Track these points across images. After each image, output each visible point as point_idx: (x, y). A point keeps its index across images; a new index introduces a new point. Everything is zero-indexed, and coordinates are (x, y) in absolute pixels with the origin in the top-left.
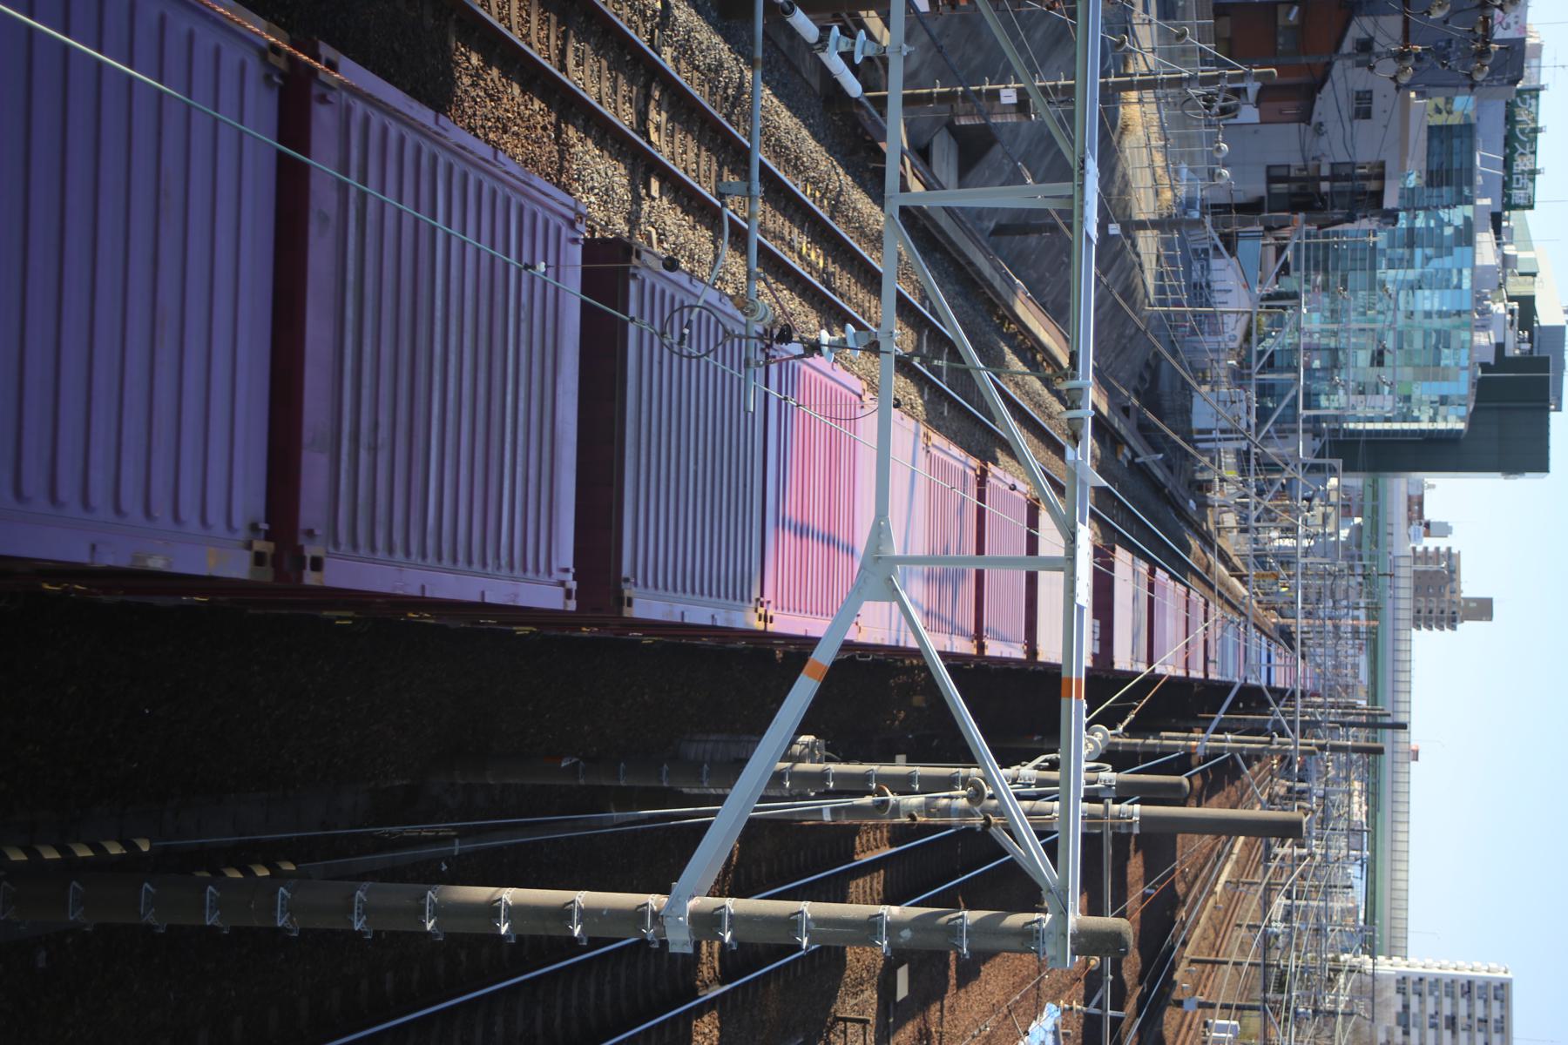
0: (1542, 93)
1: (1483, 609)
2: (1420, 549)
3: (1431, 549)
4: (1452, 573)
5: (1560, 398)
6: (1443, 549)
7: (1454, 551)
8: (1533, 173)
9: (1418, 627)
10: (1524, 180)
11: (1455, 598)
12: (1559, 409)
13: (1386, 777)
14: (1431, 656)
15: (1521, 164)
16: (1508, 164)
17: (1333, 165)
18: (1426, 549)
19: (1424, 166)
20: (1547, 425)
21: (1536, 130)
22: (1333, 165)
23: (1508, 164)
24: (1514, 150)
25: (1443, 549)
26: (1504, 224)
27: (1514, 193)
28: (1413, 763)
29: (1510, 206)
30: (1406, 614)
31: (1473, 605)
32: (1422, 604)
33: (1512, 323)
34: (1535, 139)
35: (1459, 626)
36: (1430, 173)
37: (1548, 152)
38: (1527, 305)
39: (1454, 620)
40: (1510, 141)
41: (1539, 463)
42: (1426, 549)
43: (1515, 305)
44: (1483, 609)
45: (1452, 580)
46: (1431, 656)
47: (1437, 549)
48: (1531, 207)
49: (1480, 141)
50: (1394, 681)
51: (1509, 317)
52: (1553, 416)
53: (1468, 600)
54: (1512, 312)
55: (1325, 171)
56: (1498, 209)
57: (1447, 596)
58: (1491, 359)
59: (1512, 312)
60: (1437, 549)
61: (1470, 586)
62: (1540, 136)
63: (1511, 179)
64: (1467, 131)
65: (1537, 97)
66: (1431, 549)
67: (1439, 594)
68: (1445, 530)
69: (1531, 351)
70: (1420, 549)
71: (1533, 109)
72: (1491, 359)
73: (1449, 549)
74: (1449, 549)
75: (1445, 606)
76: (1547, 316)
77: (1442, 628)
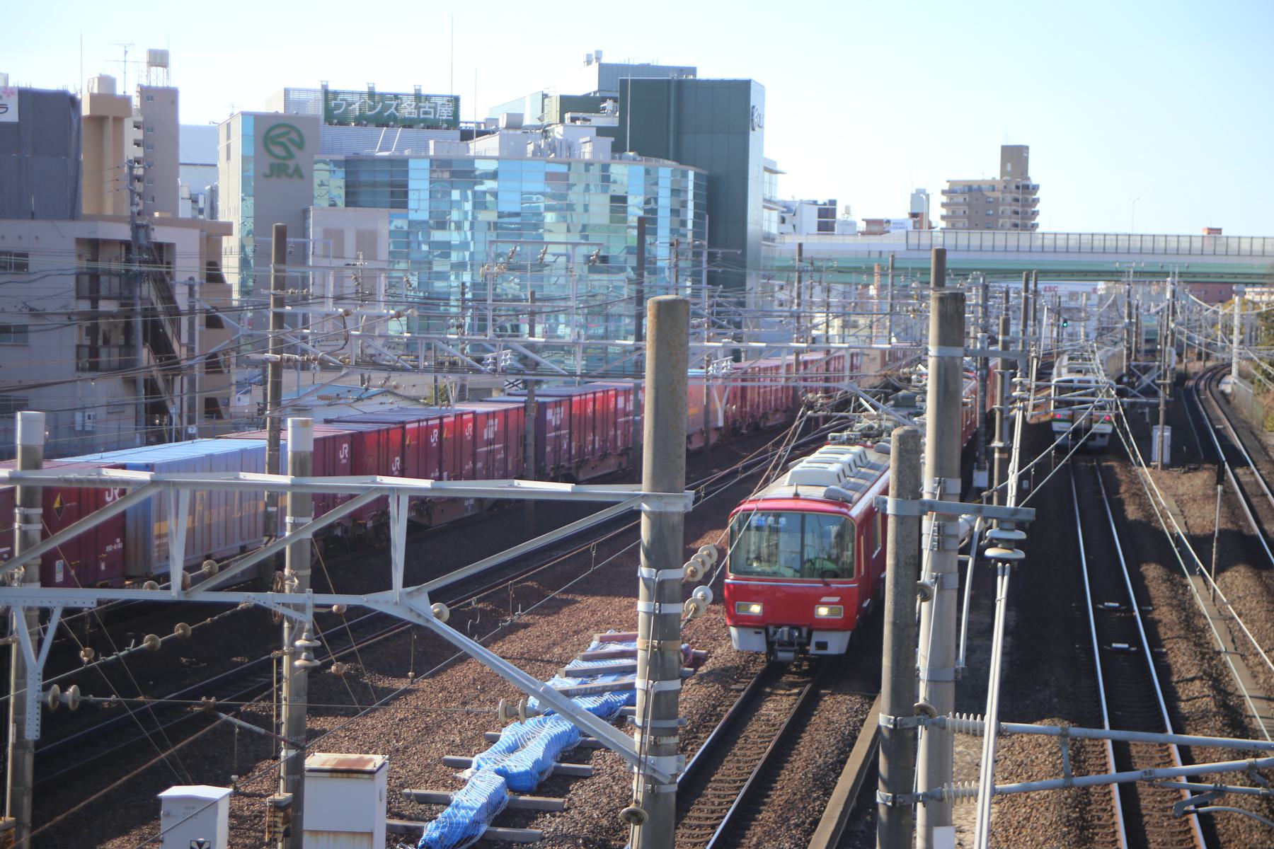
0: (331, 88)
1: (1015, 157)
2: (943, 224)
3: (944, 212)
4: (259, 118)
5: (681, 70)
6: (944, 199)
7: (946, 187)
8: (418, 97)
9: (1035, 226)
10: (426, 106)
11: (1001, 187)
12: (693, 71)
13: (1244, 265)
14: (1062, 214)
15: (408, 110)
16: (408, 124)
17: (79, 297)
18: (943, 218)
19: (384, 212)
20: (708, 81)
21: (371, 94)
22: (79, 297)
23: (408, 124)
24: (393, 117)
25: (944, 199)
26: (483, 128)
27: (437, 117)
28: (1224, 233)
29: (454, 122)
30: (1013, 239)
31: (1009, 167)
32: (1008, 223)
33: (585, 119)
34: (382, 95)
35: (1034, 181)
36: (393, 205)
37: (396, 79)
38: (568, 104)
39: (1026, 187)
40: (382, 121)
41: (741, 89)
42: (943, 218)
43: (568, 116)
44: (1015, 157)
45: (980, 189)
46: (1062, 214)
47: (943, 205)
48: (456, 100)
49: (366, 152)
50: (1141, 252)
51: (578, 123)
52: (702, 75)
53: (1003, 173)
54: (573, 120)
55: (85, 306)
56: (457, 134)
57: (998, 194)
58: (609, 141)
59: (573, 120)
60: (943, 205)
61: (988, 169)
62: (378, 90)
63: (424, 120)
64: (352, 166)
65: (336, 93)
66: (944, 212)
67: (995, 203)
68: (920, 197)
69: (615, 100)
70: (943, 224)
71: (349, 98)
72: (609, 141)
73: (944, 192)
74: (944, 192)
75: (1009, 198)
76: (586, 83)
77: (1036, 201)
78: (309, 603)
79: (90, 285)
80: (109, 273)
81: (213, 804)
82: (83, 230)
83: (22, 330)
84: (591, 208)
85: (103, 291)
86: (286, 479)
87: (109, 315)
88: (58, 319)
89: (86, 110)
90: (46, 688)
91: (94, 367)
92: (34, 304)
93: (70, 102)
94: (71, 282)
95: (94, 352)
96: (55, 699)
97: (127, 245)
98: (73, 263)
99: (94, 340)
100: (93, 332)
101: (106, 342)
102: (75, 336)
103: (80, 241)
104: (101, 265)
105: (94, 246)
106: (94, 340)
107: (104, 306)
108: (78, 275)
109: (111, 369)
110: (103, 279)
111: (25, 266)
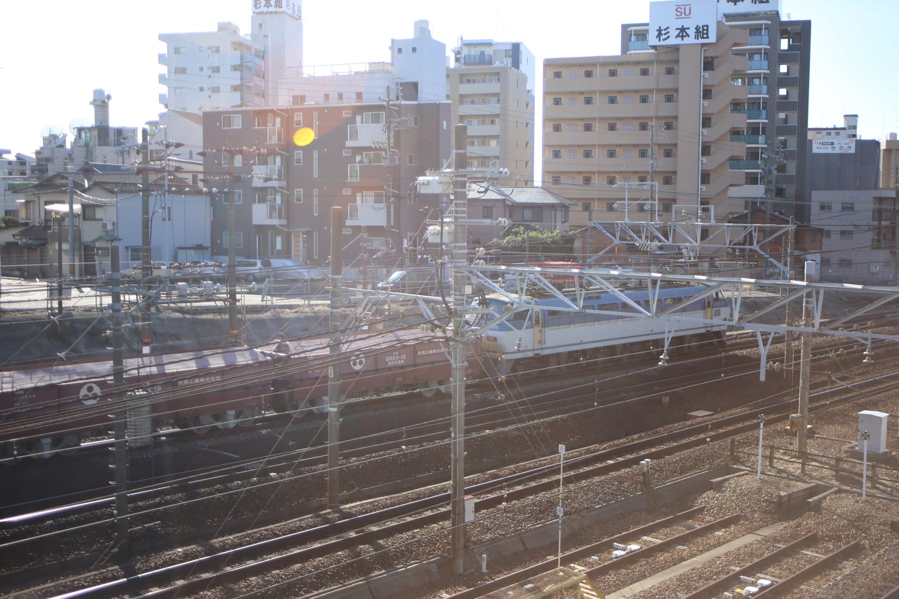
55: (876, 223)
78: (870, 338)
79: (878, 215)
80: (886, 210)
81: (880, 419)
82: (876, 194)
83: (851, 233)
84: (344, 96)
85: (884, 217)
86: (804, 283)
87: (886, 227)
88: (864, 228)
89: (883, 146)
90: (767, 362)
91: (879, 248)
92: (856, 223)
93: (876, 144)
94: (871, 214)
95: (879, 241)
96: (770, 367)
97: (894, 199)
98: (871, 206)
99: (879, 237)
100: (879, 234)
101: (884, 238)
102: (870, 235)
103: (875, 198)
104: (883, 206)
105: (880, 200)
106: (879, 237)
107: (884, 223)
108: (874, 211)
109: (885, 248)
110: (884, 213)
111: (853, 208)
